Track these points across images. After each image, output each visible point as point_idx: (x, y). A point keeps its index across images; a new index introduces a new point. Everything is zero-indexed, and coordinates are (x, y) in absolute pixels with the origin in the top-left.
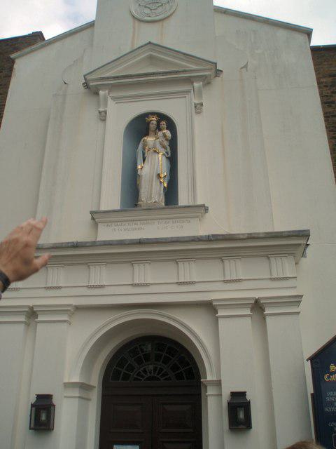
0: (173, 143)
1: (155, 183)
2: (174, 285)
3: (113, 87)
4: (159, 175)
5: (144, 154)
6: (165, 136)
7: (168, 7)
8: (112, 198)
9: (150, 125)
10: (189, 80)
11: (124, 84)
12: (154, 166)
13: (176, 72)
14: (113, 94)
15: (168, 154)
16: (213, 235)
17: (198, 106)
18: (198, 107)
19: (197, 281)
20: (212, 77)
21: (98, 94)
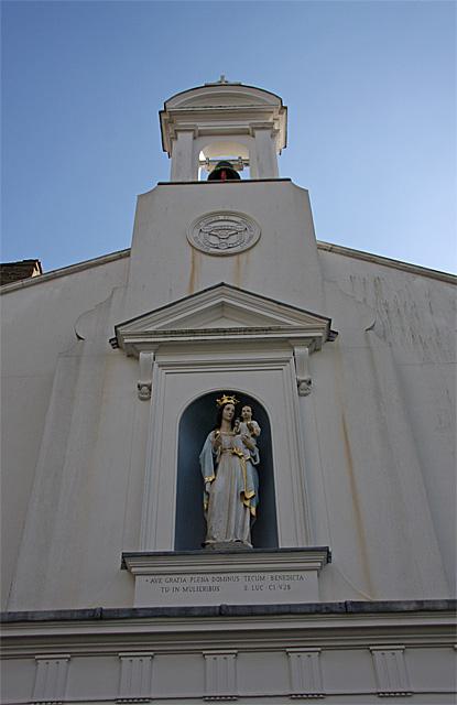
0: (264, 444)
1: (237, 506)
2: (287, 699)
3: (159, 348)
4: (243, 493)
5: (215, 459)
6: (250, 428)
7: (246, 235)
8: (163, 537)
9: (225, 411)
10: (286, 343)
11: (174, 343)
12: (230, 479)
13: (269, 330)
14: (162, 359)
15: (255, 458)
16: (352, 603)
17: (304, 384)
18: (304, 387)
19: (241, 694)
20: (324, 339)
21: (138, 358)
